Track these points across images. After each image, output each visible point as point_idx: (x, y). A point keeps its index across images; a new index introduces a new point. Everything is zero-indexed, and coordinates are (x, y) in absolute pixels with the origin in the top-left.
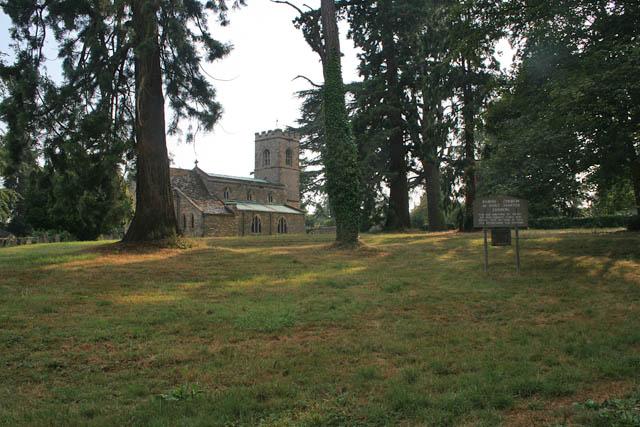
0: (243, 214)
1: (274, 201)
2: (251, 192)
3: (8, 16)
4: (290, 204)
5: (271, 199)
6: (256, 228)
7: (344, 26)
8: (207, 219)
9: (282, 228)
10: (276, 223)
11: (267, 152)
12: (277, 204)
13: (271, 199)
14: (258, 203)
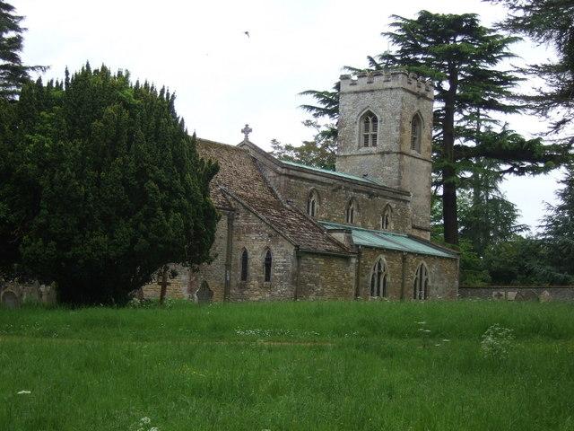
1: (392, 225)
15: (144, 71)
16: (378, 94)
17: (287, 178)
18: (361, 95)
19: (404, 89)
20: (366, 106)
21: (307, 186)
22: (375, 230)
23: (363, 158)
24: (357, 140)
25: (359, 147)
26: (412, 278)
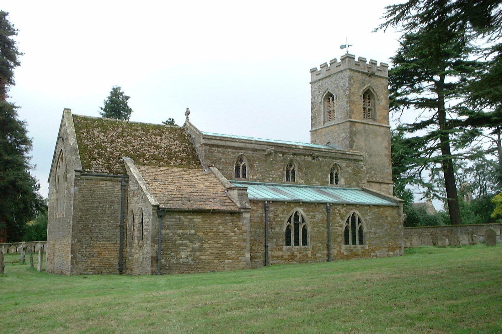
0: (266, 208)
1: (342, 181)
2: (245, 162)
3: (415, 137)
4: (374, 188)
5: (335, 179)
6: (296, 233)
7: (500, 118)
8: (170, 220)
9: (354, 234)
10: (340, 225)
11: (329, 97)
12: (349, 186)
13: (335, 179)
14: (308, 184)
15: (20, 42)
16: (334, 78)
17: (208, 147)
18: (323, 81)
19: (351, 70)
20: (326, 88)
21: (234, 153)
22: (273, 184)
23: (327, 129)
24: (322, 116)
25: (324, 122)
26: (341, 226)
